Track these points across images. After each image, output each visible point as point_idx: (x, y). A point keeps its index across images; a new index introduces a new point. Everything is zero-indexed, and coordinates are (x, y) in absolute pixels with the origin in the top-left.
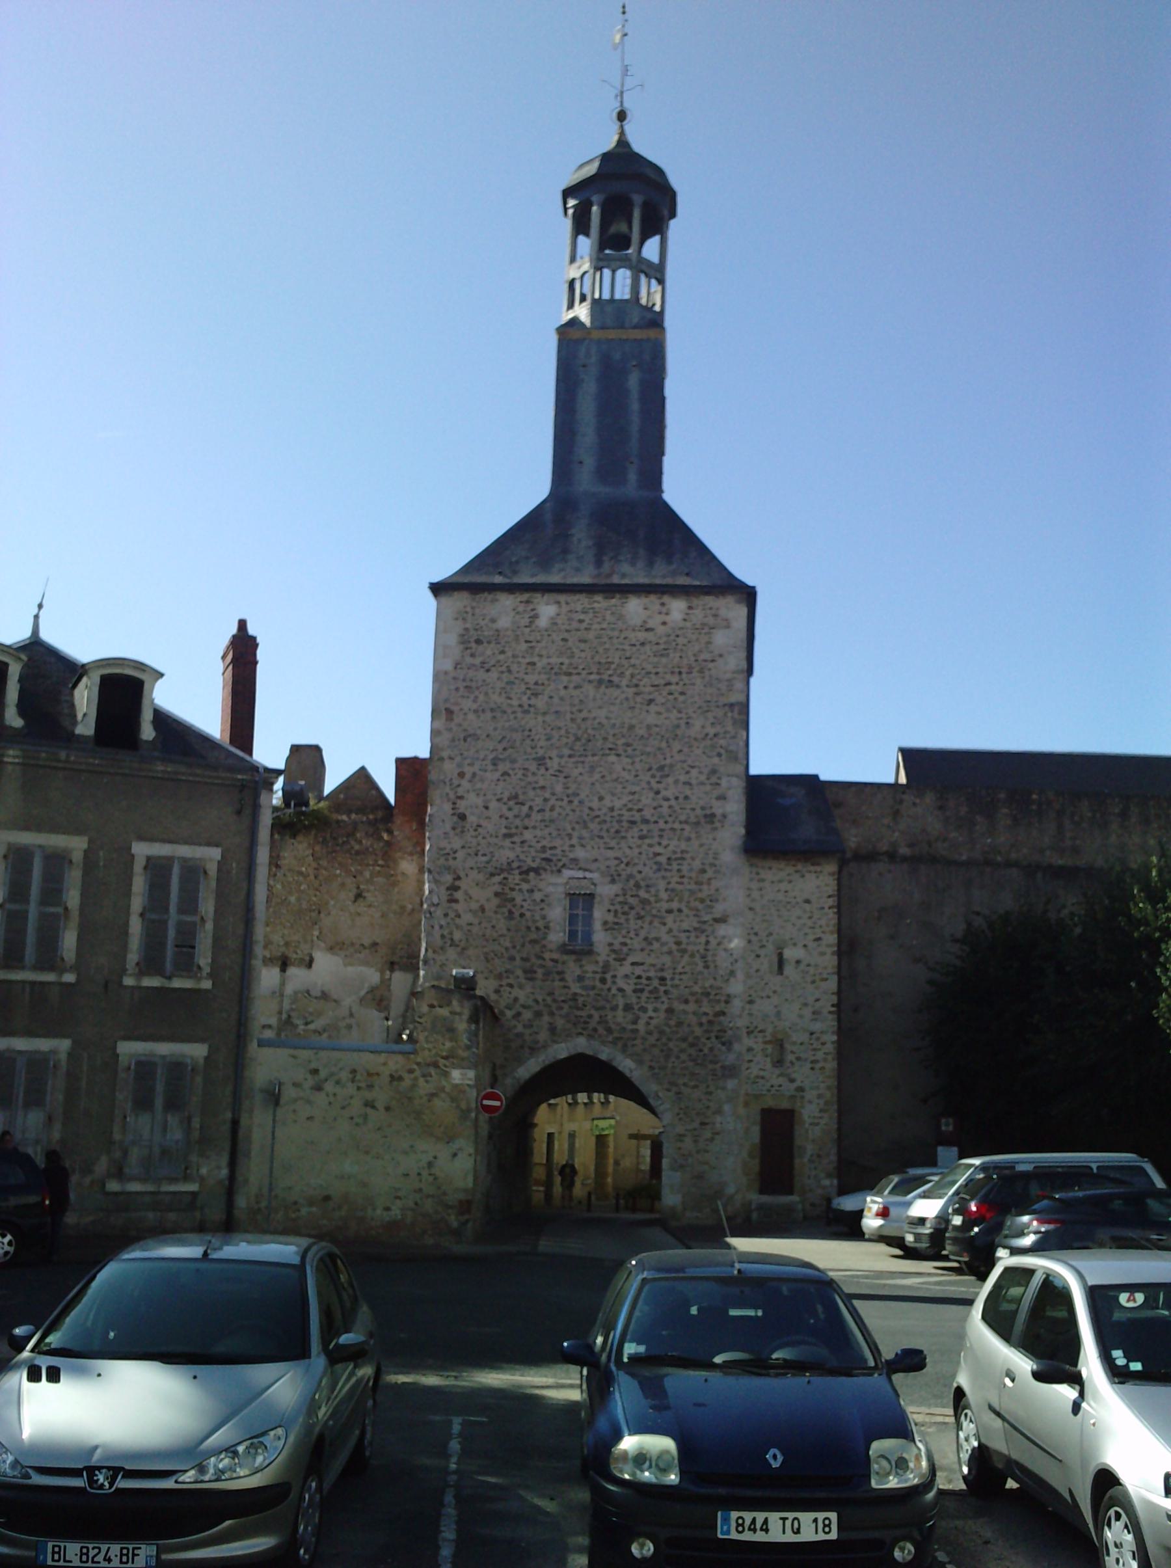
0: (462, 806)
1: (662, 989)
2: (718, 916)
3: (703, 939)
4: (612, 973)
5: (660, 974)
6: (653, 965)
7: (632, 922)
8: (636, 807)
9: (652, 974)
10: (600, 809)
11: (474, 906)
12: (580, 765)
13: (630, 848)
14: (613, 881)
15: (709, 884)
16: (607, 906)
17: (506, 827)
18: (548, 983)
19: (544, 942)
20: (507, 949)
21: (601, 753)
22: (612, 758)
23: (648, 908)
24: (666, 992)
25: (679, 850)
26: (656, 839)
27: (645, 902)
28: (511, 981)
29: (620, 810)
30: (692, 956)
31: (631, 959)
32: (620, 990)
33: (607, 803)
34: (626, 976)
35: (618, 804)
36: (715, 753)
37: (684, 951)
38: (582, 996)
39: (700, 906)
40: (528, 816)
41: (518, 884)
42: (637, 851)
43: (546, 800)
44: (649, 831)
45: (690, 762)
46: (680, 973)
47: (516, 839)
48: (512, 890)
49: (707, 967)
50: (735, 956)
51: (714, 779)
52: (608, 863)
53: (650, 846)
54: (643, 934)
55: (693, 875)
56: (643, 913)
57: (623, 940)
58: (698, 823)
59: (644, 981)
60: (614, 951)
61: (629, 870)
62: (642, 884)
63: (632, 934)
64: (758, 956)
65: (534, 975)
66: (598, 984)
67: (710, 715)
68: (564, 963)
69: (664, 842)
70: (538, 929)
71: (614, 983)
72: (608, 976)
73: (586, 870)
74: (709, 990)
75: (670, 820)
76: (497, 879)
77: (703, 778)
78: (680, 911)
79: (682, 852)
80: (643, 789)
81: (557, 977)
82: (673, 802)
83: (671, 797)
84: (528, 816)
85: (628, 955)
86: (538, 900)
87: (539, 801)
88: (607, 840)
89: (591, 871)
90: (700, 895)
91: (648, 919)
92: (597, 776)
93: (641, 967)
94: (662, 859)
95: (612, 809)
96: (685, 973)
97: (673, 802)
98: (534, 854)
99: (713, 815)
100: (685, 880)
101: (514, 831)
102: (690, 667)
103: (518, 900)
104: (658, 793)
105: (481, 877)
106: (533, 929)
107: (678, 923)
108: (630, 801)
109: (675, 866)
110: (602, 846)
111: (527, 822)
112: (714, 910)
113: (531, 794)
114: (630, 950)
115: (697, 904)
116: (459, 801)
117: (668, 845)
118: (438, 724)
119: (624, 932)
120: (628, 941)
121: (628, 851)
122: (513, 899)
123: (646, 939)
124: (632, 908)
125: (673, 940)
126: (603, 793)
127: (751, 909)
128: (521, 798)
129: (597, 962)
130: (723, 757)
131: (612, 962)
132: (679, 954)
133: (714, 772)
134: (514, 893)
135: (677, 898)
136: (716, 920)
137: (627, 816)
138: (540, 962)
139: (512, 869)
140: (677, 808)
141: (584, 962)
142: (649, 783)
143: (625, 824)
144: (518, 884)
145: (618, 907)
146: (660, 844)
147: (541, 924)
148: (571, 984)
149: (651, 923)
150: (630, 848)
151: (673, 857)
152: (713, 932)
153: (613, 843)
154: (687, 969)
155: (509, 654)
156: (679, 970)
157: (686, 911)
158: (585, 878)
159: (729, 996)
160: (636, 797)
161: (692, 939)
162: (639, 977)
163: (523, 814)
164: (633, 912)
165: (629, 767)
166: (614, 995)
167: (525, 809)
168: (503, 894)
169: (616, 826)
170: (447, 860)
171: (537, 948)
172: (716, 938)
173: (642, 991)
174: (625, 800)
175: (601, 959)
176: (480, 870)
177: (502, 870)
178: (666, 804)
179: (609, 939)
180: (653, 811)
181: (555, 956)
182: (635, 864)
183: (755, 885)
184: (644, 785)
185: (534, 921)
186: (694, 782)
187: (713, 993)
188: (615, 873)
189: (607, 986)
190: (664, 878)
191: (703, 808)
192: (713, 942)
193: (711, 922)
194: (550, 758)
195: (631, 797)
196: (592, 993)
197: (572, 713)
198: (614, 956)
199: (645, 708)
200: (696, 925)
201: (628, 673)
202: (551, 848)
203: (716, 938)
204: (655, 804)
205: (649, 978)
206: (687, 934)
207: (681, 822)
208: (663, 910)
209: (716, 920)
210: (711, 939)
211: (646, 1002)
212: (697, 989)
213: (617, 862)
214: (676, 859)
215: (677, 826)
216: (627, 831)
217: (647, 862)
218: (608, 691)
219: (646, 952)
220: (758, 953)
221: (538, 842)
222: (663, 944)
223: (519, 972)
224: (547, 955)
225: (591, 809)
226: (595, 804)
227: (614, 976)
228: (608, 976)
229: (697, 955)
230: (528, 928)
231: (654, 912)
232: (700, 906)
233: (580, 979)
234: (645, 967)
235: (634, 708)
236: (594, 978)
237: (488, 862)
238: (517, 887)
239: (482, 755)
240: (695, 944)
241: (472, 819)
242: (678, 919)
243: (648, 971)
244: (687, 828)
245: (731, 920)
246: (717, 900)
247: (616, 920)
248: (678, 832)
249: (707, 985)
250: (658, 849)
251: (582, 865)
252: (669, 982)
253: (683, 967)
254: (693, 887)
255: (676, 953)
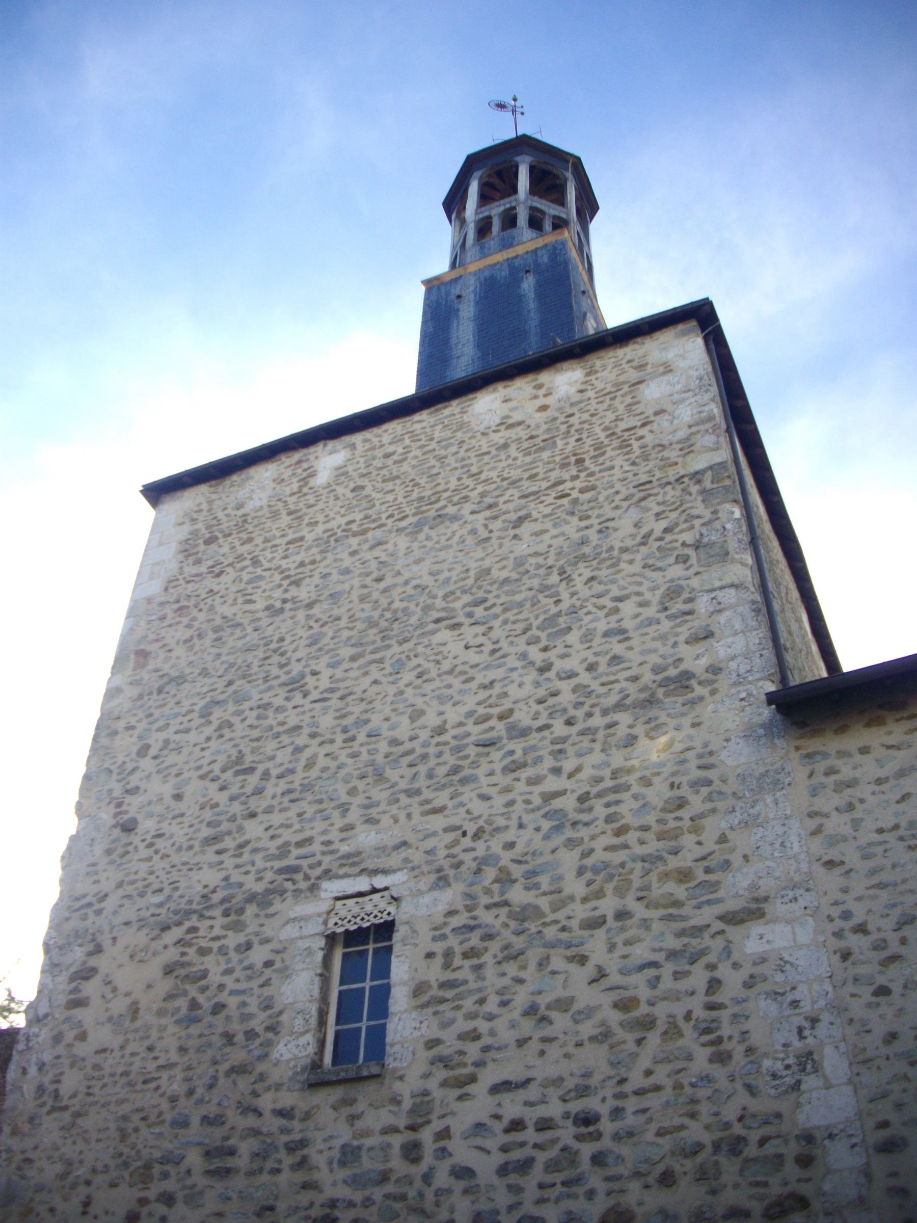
0: (133, 804)
1: (587, 1150)
2: (732, 905)
3: (699, 978)
4: (437, 1125)
5: (575, 1106)
6: (558, 1081)
7: (490, 972)
8: (496, 711)
9: (554, 1109)
10: (412, 739)
11: (119, 1005)
12: (373, 668)
13: (485, 798)
14: (442, 881)
15: (696, 830)
16: (425, 941)
17: (209, 824)
18: (265, 1177)
19: (261, 1067)
20: (174, 1100)
21: (419, 632)
22: (444, 635)
23: (533, 927)
24: (598, 1159)
25: (607, 773)
26: (549, 762)
27: (525, 914)
28: (170, 1185)
29: (461, 724)
30: (673, 1031)
31: (490, 1076)
32: (463, 1173)
33: (432, 720)
34: (479, 1127)
35: (453, 715)
36: (672, 560)
37: (648, 1023)
38: (351, 1204)
39: (680, 891)
40: (259, 791)
41: (217, 938)
42: (499, 801)
43: (298, 750)
44: (525, 752)
45: (615, 592)
46: (639, 1093)
47: (229, 843)
48: (203, 952)
49: (722, 1058)
50: (806, 1007)
51: (678, 606)
52: (430, 844)
53: (534, 781)
54: (521, 998)
55: (650, 819)
56: (519, 942)
57: (470, 1025)
58: (650, 702)
59: (530, 1135)
60: (444, 1062)
61: (481, 848)
62: (517, 871)
63: (492, 1005)
64: (883, 991)
65: (230, 1162)
66: (398, 1164)
67: (651, 503)
68: (307, 1116)
69: (568, 765)
70: (251, 1035)
71: (443, 1153)
72: (426, 1136)
73: (375, 872)
74: (737, 1129)
75: (579, 713)
76: (177, 933)
77: (651, 612)
78: (622, 915)
79: (615, 774)
80: (513, 669)
81: (288, 1160)
82: (584, 678)
83: (580, 669)
84: (259, 791)
85: (479, 1064)
86: (259, 964)
87: (283, 756)
88: (427, 794)
89: (385, 872)
90: (674, 863)
91: (534, 955)
92: (408, 676)
93: (522, 1095)
94: (568, 803)
95: (440, 730)
96: (657, 1088)
97: (584, 678)
98: (260, 864)
99: (687, 675)
100: (632, 837)
101: (225, 827)
102: (599, 448)
103: (215, 978)
104: (545, 669)
105: (141, 938)
106: (240, 1038)
107: (621, 950)
108: (479, 704)
109: (600, 810)
110: (416, 811)
111: (253, 803)
112: (721, 894)
113: (269, 746)
114: (486, 1049)
115: (671, 887)
116: (128, 799)
117: (578, 769)
118: (119, 680)
119: (469, 1004)
120: (483, 1026)
121: (478, 807)
122: (204, 974)
123: (531, 1011)
124: (489, 937)
125: (607, 999)
126: (420, 702)
127: (830, 864)
128: (248, 759)
129: (396, 1101)
130: (693, 560)
131: (438, 1094)
132: (630, 1038)
133: (674, 592)
134: (206, 959)
135: (609, 888)
136: (733, 919)
137: (475, 730)
138: (251, 1121)
139: (212, 907)
140: (595, 685)
141: (360, 1107)
142: (523, 656)
143: (472, 751)
144: (217, 938)
145: (453, 941)
146: (557, 771)
147: (258, 1023)
148: (323, 1175)
149: (542, 964)
150: (485, 798)
151: (594, 791)
152: (727, 951)
153: (442, 798)
154: (661, 1076)
155: (259, 540)
156: (637, 1080)
157: (639, 911)
158: (375, 891)
159: (808, 1138)
160: (497, 690)
161: (667, 983)
162: (517, 1125)
163: (249, 790)
164: (494, 947)
165: (481, 640)
166: (439, 1192)
167: (253, 780)
168: (183, 965)
169: (451, 760)
170: (84, 918)
171: (244, 1084)
172: (736, 966)
173: (525, 1165)
174: (470, 702)
175: (405, 1090)
176: (142, 923)
177: (188, 913)
178: (565, 686)
179: (430, 1030)
180: (536, 707)
181: (287, 1099)
182: (498, 830)
183: (828, 801)
184: (512, 662)
185: (246, 1018)
186: (628, 624)
187: (754, 1136)
188: (446, 864)
189: (423, 1167)
190: (571, 843)
191: (656, 670)
192: (732, 980)
193: (718, 925)
194: (315, 673)
195: (483, 695)
196: (377, 1193)
197: (345, 731)
198: (442, 1074)
199: (512, 532)
200: (673, 943)
201: (474, 495)
202: (299, 844)
203: (736, 966)
204: (541, 692)
205: (544, 1125)
206: (651, 972)
207: (605, 712)
208: (574, 924)
209: (733, 919)
210: (724, 972)
211: (541, 1201)
212: (696, 1132)
213: (449, 837)
214: (599, 795)
215: (597, 721)
216: (475, 765)
217: (526, 819)
218: (441, 529)
219: (534, 1046)
220: (881, 980)
221: (273, 837)
222: (588, 1013)
223: (194, 1158)
224: (266, 1102)
225: (395, 742)
226: (404, 729)
227: (444, 1134)
228: (426, 1136)
229: (687, 1029)
230: (229, 1038)
231: (551, 933)
232: (680, 891)
233: (349, 1155)
234: (533, 1092)
235: (487, 539)
236: (386, 1148)
237: (161, 905)
238: (215, 945)
239: (186, 705)
240: (676, 997)
241: (147, 825)
242: (619, 939)
243: (543, 1101)
244: (624, 718)
245: (778, 908)
246: (726, 865)
247: (449, 976)
248: (600, 735)
249: (730, 1113)
250: (552, 784)
251: (370, 864)
252: (606, 1126)
253: (648, 1073)
254: (653, 846)
255: (620, 1034)
